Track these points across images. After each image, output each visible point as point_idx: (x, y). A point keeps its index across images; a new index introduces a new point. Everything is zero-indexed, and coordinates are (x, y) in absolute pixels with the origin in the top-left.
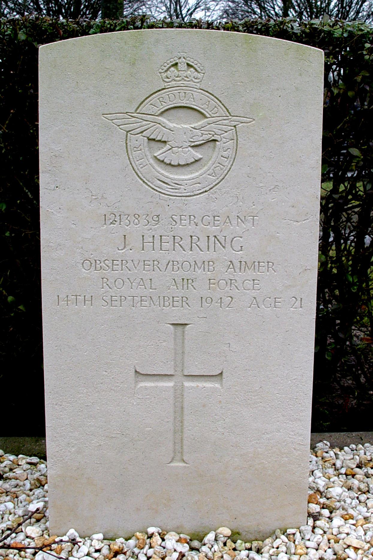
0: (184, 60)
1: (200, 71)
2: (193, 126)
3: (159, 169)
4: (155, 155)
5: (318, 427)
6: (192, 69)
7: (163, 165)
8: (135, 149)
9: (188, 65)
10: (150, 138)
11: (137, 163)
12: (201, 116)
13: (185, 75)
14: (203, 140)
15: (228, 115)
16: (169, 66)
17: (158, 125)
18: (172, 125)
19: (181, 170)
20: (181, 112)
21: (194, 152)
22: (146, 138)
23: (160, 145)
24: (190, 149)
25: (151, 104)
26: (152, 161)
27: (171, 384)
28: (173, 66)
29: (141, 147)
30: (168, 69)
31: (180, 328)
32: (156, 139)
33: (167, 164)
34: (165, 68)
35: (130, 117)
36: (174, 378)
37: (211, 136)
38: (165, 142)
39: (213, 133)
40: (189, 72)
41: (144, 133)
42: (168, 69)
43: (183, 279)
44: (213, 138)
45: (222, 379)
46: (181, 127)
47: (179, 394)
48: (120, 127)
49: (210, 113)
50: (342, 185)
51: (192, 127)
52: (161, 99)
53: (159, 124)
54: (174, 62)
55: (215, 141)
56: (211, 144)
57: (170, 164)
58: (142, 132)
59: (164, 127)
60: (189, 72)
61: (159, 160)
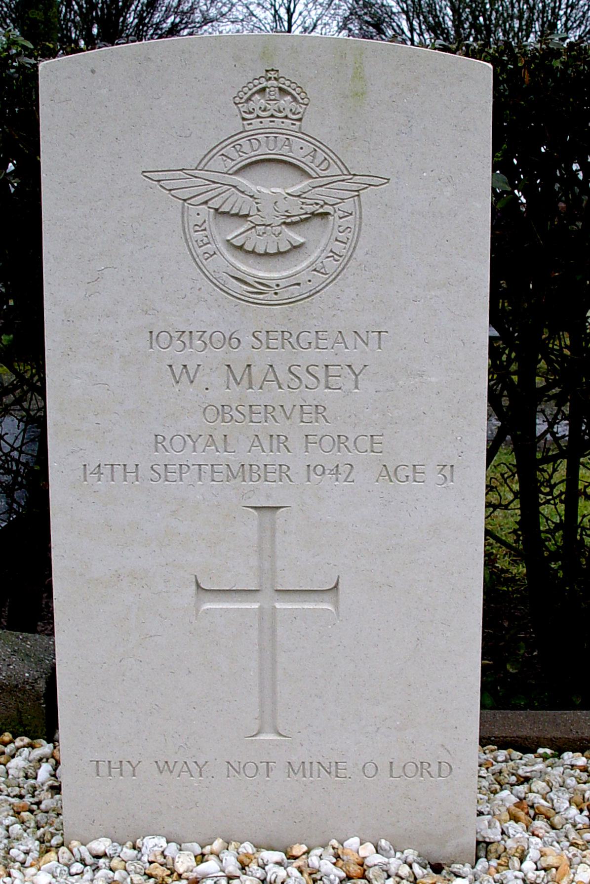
0: (275, 82)
1: (301, 101)
2: (289, 191)
3: (232, 260)
4: (229, 238)
5: (501, 688)
6: (289, 98)
7: (241, 255)
8: (197, 228)
9: (280, 89)
10: (225, 208)
11: (200, 251)
12: (299, 173)
13: (276, 107)
14: (306, 213)
15: (346, 172)
16: (250, 92)
17: (233, 189)
18: (253, 188)
19: (251, 259)
20: (277, 169)
21: (291, 234)
22: (212, 210)
23: (241, 220)
24: (283, 227)
25: (223, 155)
26: (223, 250)
27: (256, 606)
28: (257, 92)
29: (206, 225)
30: (249, 99)
31: (268, 513)
32: (241, 214)
33: (249, 252)
34: (246, 97)
35: (207, 182)
36: (258, 595)
37: (318, 207)
38: (247, 216)
39: (322, 203)
40: (282, 102)
41: (210, 202)
42: (249, 99)
43: (271, 436)
44: (321, 210)
45: (337, 595)
46: (273, 190)
47: (268, 622)
48: (172, 192)
49: (317, 169)
50: (11, 164)
51: (288, 194)
52: (238, 147)
53: (234, 187)
54: (261, 86)
55: (327, 214)
56: (317, 221)
57: (253, 252)
58: (206, 203)
59: (243, 192)
60: (282, 102)
61: (232, 245)
